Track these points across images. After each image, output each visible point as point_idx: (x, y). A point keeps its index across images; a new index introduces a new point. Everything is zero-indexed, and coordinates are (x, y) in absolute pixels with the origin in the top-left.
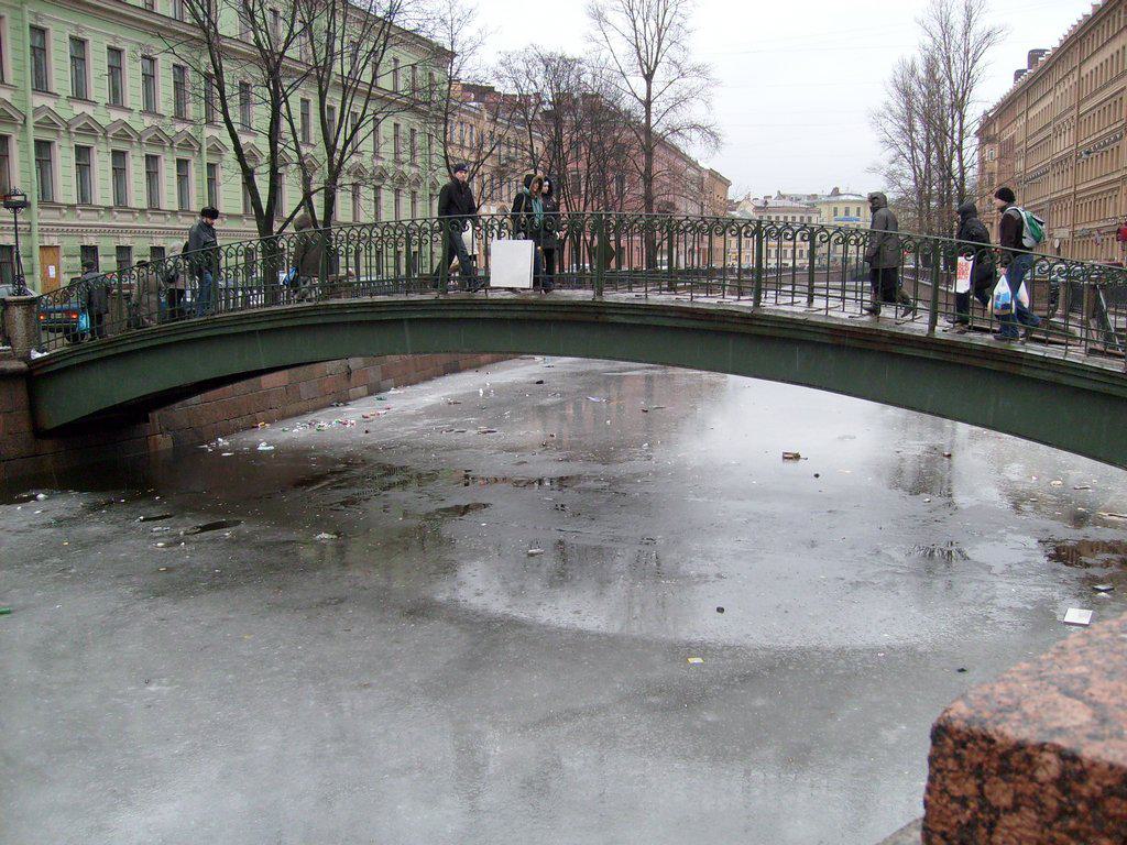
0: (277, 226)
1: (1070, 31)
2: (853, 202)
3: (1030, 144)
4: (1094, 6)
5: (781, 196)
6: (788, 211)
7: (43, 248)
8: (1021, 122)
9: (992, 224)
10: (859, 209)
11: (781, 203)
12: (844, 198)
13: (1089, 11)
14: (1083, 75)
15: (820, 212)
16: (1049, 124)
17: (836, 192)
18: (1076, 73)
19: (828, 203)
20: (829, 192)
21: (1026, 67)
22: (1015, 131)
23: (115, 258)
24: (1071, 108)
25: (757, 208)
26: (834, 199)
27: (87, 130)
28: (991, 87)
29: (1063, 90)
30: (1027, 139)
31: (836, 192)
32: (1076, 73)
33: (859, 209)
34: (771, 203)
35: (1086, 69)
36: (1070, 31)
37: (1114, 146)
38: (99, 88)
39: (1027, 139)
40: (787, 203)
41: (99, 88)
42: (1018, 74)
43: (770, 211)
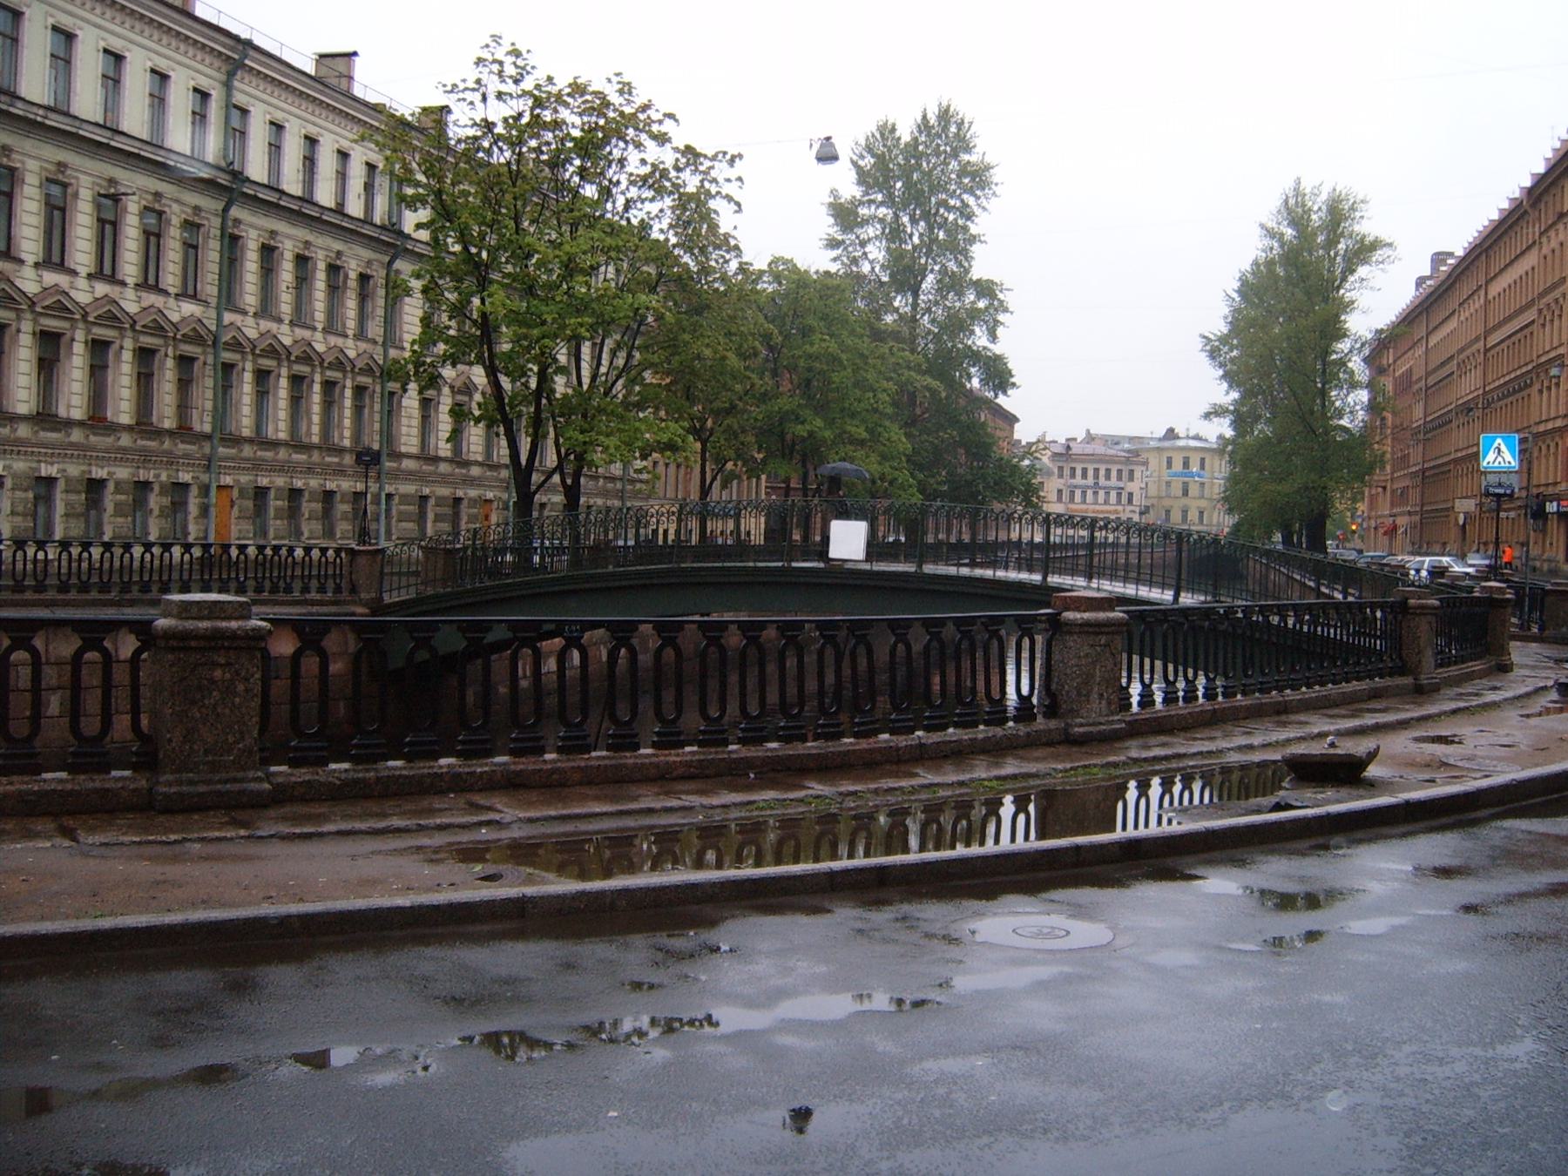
0: (536, 478)
1: (1555, 150)
2: (1196, 449)
3: (1431, 381)
4: (1501, 210)
5: (1090, 438)
6: (1100, 461)
7: (219, 487)
8: (1420, 351)
9: (1384, 488)
10: (1203, 460)
11: (1089, 449)
12: (1181, 443)
13: (1496, 216)
14: (1490, 297)
15: (1146, 463)
16: (1452, 357)
17: (1171, 434)
18: (1482, 292)
19: (1158, 449)
20: (1161, 433)
21: (1428, 273)
22: (1412, 362)
23: (83, 496)
24: (1477, 339)
25: (1055, 455)
26: (1167, 444)
27: (108, 319)
28: (1376, 301)
29: (1554, 244)
30: (1428, 374)
31: (1171, 434)
32: (1482, 292)
33: (1203, 460)
34: (1076, 449)
35: (1495, 288)
36: (1555, 150)
37: (1525, 393)
38: (82, 253)
39: (1428, 374)
40: (1099, 449)
41: (82, 253)
42: (1420, 281)
43: (1075, 461)
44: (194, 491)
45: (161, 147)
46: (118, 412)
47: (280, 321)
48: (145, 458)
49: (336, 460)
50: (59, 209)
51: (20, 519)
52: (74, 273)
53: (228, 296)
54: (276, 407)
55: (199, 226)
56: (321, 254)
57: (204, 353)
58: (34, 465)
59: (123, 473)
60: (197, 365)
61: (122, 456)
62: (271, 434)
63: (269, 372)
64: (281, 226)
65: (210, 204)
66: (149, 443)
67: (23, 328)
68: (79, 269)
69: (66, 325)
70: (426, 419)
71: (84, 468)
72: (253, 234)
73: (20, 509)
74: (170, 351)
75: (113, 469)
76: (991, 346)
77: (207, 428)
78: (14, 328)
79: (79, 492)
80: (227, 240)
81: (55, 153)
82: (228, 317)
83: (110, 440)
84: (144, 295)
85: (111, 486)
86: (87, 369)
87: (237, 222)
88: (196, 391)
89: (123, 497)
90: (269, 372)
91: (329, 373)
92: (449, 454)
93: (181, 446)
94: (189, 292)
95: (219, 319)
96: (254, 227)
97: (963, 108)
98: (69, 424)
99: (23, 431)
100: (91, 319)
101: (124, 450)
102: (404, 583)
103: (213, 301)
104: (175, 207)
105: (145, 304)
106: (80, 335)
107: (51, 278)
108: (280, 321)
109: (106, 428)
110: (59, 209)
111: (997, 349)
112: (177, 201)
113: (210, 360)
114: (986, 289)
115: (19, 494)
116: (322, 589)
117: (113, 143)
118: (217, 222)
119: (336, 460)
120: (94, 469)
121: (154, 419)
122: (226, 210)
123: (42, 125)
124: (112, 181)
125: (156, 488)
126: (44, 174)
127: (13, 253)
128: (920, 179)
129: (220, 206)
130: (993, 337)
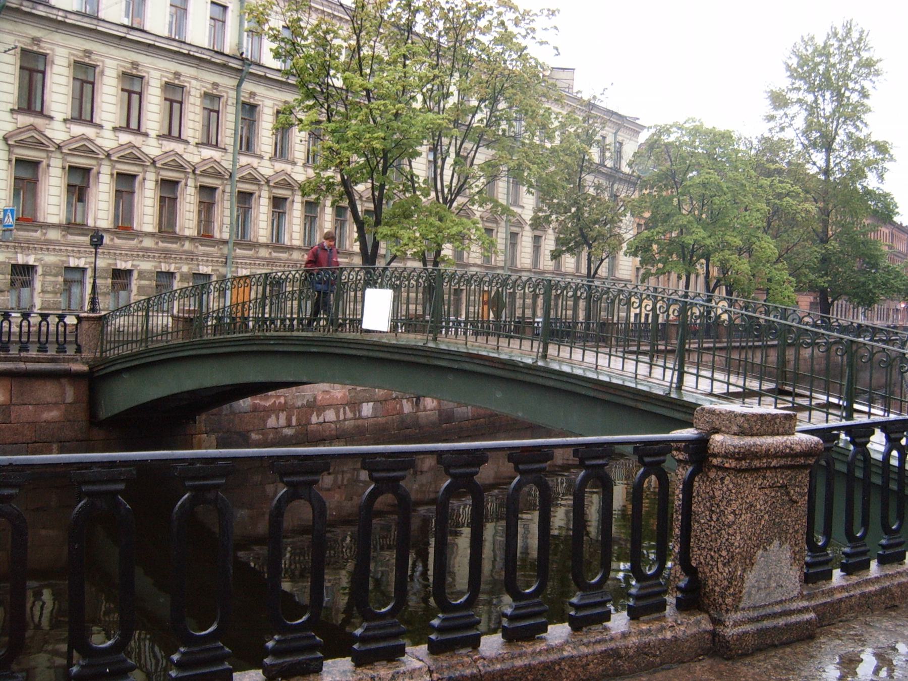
23: (110, 281)
27: (84, 151)
44: (89, 273)
45: (184, 43)
46: (142, 223)
47: (294, 163)
48: (167, 255)
49: (346, 260)
50: (215, 111)
51: (50, 296)
52: (187, 142)
53: (247, 145)
54: (291, 223)
55: (219, 97)
56: (269, 103)
57: (222, 184)
58: (64, 259)
59: (147, 266)
60: (218, 193)
61: (145, 253)
62: (287, 241)
63: (517, 234)
64: (187, 71)
65: (227, 82)
66: (170, 245)
67: (189, 184)
68: (150, 132)
69: (93, 162)
70: (537, 248)
71: (10, 255)
72: (155, 74)
73: (50, 289)
74: (228, 189)
75: (135, 263)
76: (881, 186)
77: (226, 236)
78: (257, 194)
79: (106, 278)
80: (240, 107)
81: (80, 44)
82: (244, 160)
83: (134, 243)
84: (165, 143)
85: (135, 275)
86: (113, 194)
87: (253, 94)
88: (217, 210)
89: (147, 282)
90: (517, 234)
91: (275, 191)
92: (551, 268)
93: (201, 248)
94: (210, 141)
95: (234, 162)
96: (156, 72)
97: (861, 23)
98: (291, 248)
99: (53, 235)
100: (271, 184)
101: (147, 250)
102: (112, 346)
103: (230, 149)
104: (194, 82)
105: (167, 149)
106: (191, 182)
107: (279, 166)
108: (294, 163)
109: (131, 234)
110: (215, 111)
111: (886, 188)
112: (196, 79)
113: (228, 189)
114: (882, 148)
115: (50, 278)
116: (43, 349)
117: (129, 36)
118: (233, 94)
119: (346, 260)
120: (118, 262)
121: (135, 226)
122: (239, 85)
123: (64, 23)
124: (135, 65)
125: (178, 276)
126: (276, 107)
127: (45, 113)
128: (831, 76)
129: (234, 82)
130: (881, 177)
